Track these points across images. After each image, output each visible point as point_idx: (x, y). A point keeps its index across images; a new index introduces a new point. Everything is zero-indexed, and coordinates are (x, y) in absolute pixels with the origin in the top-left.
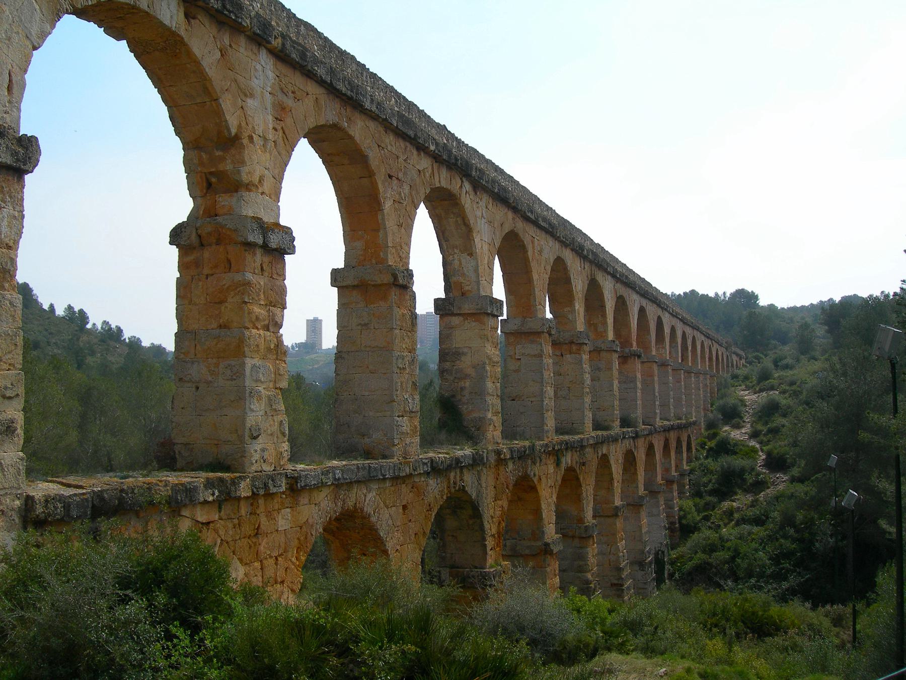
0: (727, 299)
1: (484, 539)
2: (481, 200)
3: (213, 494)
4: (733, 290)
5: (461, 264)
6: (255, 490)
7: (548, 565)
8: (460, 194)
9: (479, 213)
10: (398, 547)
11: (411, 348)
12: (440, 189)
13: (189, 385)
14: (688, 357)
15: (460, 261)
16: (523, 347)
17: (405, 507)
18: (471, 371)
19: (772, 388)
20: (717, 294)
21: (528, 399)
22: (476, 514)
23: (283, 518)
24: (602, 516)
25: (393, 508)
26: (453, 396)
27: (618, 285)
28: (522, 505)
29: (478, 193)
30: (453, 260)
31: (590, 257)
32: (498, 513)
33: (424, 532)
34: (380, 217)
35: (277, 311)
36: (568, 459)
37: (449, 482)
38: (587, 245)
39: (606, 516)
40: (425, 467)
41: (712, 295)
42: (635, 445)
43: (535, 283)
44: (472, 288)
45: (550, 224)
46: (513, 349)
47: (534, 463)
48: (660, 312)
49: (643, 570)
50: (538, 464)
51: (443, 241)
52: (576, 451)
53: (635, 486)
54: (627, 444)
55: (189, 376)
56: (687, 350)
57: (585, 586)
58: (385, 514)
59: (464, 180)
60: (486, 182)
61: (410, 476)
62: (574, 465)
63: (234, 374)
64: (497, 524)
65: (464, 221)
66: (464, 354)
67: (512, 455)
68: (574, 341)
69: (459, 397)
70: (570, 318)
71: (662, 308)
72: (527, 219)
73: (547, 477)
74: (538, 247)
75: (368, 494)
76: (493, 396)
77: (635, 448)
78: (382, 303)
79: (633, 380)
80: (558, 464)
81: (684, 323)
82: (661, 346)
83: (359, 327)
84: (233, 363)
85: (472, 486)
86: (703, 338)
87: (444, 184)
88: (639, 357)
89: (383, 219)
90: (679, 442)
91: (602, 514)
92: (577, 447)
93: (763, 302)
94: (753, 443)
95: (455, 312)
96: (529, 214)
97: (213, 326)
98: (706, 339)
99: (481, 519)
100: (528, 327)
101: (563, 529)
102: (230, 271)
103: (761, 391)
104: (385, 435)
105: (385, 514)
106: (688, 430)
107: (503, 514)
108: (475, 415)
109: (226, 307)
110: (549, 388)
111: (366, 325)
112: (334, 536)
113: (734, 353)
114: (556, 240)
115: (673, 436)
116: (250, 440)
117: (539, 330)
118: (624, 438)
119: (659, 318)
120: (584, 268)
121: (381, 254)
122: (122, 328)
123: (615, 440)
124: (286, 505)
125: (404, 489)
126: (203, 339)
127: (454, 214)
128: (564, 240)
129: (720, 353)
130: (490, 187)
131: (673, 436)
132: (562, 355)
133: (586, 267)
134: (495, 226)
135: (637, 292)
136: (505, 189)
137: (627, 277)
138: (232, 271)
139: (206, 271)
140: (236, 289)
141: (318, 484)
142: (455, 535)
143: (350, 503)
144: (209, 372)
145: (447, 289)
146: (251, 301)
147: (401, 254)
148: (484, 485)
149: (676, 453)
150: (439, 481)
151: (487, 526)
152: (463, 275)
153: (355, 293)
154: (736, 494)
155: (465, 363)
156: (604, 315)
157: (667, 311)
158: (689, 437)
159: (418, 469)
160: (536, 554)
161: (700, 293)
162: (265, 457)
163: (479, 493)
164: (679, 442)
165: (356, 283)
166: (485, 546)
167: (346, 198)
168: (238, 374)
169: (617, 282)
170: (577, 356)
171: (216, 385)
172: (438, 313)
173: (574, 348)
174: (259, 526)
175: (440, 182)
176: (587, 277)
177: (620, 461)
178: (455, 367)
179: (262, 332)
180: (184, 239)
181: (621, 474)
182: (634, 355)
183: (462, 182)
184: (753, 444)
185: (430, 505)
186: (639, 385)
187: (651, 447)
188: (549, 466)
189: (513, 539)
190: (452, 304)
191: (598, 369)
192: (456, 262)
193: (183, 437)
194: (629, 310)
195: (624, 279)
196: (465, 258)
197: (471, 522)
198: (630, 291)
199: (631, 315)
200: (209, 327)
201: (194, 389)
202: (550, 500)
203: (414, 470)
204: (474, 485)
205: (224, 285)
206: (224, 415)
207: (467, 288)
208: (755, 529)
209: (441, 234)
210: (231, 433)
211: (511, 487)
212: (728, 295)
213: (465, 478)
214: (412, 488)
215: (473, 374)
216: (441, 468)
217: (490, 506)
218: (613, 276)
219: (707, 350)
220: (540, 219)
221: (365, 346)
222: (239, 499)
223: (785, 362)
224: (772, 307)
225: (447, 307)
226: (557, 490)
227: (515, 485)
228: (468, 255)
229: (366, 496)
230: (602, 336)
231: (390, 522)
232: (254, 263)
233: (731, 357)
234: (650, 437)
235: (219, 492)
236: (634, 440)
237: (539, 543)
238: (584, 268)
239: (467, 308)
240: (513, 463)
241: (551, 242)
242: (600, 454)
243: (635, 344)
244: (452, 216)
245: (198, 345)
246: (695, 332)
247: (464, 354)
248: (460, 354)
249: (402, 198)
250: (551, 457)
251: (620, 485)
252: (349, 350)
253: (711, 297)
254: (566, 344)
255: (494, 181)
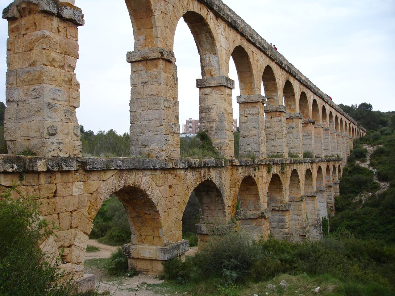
0: (357, 107)
1: (224, 208)
2: (221, 25)
3: (13, 167)
4: (360, 103)
5: (210, 60)
6: (50, 167)
7: (264, 224)
8: (206, 18)
9: (219, 32)
10: (166, 210)
11: (174, 97)
12: (193, 13)
13: (14, 103)
14: (338, 128)
15: (209, 58)
16: (248, 110)
17: (170, 187)
18: (216, 118)
19: (380, 144)
20: (352, 105)
21: (251, 137)
22: (219, 194)
23: (76, 188)
24: (294, 201)
25: (162, 187)
26: (207, 131)
27: (302, 87)
28: (249, 192)
29: (219, 21)
30: (206, 58)
31: (286, 68)
32: (233, 195)
33: (184, 202)
34: (153, 20)
35: (70, 59)
36: (275, 170)
37: (201, 175)
38: (284, 62)
39: (296, 201)
40: (183, 164)
41: (350, 106)
42: (311, 167)
43: (254, 76)
44: (216, 73)
45: (263, 46)
46: (244, 111)
47: (255, 170)
48: (324, 103)
49: (316, 229)
50: (257, 171)
51: (200, 47)
52: (279, 166)
53: (312, 187)
54: (308, 166)
55: (14, 98)
56: (338, 124)
57: (286, 236)
58: (156, 190)
59: (209, 11)
60: (223, 14)
61: (173, 169)
62: (278, 173)
63: (38, 94)
64: (232, 200)
65: (210, 34)
66: (212, 108)
67: (241, 164)
68: (278, 110)
69: (210, 132)
70: (276, 99)
71: (325, 102)
72: (249, 41)
73: (262, 178)
74: (256, 58)
75: (143, 178)
76: (229, 131)
77: (311, 168)
78: (155, 70)
79: (310, 135)
80: (269, 172)
81: (336, 111)
82: (325, 121)
83: (143, 84)
84: (37, 87)
85: (216, 179)
86: (346, 120)
87: (197, 11)
88: (313, 123)
89: (155, 21)
90: (334, 167)
91: (294, 200)
92: (279, 164)
93: (374, 109)
94: (371, 169)
95: (207, 86)
96: (250, 39)
97: (26, 66)
98: (348, 121)
99: (222, 197)
100: (251, 99)
101: (273, 206)
102: (36, 30)
103: (374, 145)
104: (158, 145)
105: (156, 190)
106: (339, 162)
107: (236, 195)
108: (219, 141)
109: (33, 53)
110: (263, 132)
111: (146, 82)
112: (128, 203)
113: (361, 129)
114: (267, 56)
115: (331, 165)
116: (48, 136)
117: (257, 101)
118: (305, 162)
119: (324, 107)
120: (283, 74)
121: (154, 42)
122: (83, 126)
123: (301, 163)
124: (79, 180)
125: (170, 177)
126: (21, 74)
127: (205, 30)
128: (271, 57)
129: (354, 128)
130: (226, 18)
131: (331, 165)
132: (272, 118)
133: (284, 74)
134: (230, 41)
135: (312, 92)
136: (235, 21)
137: (306, 83)
138: (37, 30)
139: (23, 32)
140: (39, 41)
141: (103, 168)
142: (209, 206)
143: (130, 182)
144: (24, 94)
145: (203, 74)
146: (48, 49)
147: (167, 43)
148: (223, 179)
149: (333, 173)
150: (194, 174)
151: (225, 201)
152: (211, 65)
153: (140, 64)
154: (362, 193)
155: (213, 114)
156: (294, 100)
157: (328, 104)
158: (339, 166)
159: (179, 165)
160: (257, 218)
161: (345, 105)
162: (61, 148)
163: (221, 184)
164: (334, 167)
165: (140, 59)
166: (225, 212)
167: (134, 10)
168: (39, 94)
169: (301, 85)
170: (279, 118)
171: (28, 102)
172: (198, 87)
173: (278, 113)
174: (56, 191)
175: (193, 8)
176: (285, 79)
177: (303, 174)
178: (208, 116)
179: (58, 69)
180: (10, 14)
181: (304, 180)
182: (311, 122)
183: (208, 12)
184: (371, 170)
185: (188, 187)
186: (313, 137)
187: (320, 169)
188: (263, 172)
189: (245, 210)
190: (205, 81)
191: (292, 127)
192: (207, 59)
193: (10, 136)
194: (308, 100)
195: (305, 83)
196: (212, 57)
197: (217, 199)
198: (308, 90)
199: (308, 102)
200: (24, 67)
201: (16, 106)
202: (264, 190)
203: (176, 166)
204: (217, 178)
205: (32, 39)
206: (32, 121)
207: (213, 73)
208: (374, 209)
209: (198, 43)
210: (36, 132)
211: (241, 182)
212: (358, 105)
213: (211, 174)
214: (176, 176)
215: (217, 119)
216: (195, 166)
217: (227, 190)
218: (299, 81)
219: (348, 126)
220: (257, 42)
221: (146, 95)
222: (39, 173)
223: (386, 132)
224: (378, 112)
225: (203, 84)
226: (268, 185)
227: (242, 181)
228: (214, 54)
229: (142, 178)
230: (293, 111)
231: (160, 195)
232: (52, 26)
233: (360, 131)
234: (319, 163)
235: (18, 166)
236: (311, 164)
237: (258, 212)
238: (283, 74)
239: (213, 83)
240: (242, 169)
241: (264, 56)
242: (292, 170)
243: (311, 117)
244: (203, 32)
245: (18, 79)
246: (342, 116)
247: (212, 108)
248: (210, 108)
249: (167, 11)
250: (264, 168)
251: (303, 186)
252: (138, 98)
253: (350, 107)
254: (273, 112)
255: (228, 15)
